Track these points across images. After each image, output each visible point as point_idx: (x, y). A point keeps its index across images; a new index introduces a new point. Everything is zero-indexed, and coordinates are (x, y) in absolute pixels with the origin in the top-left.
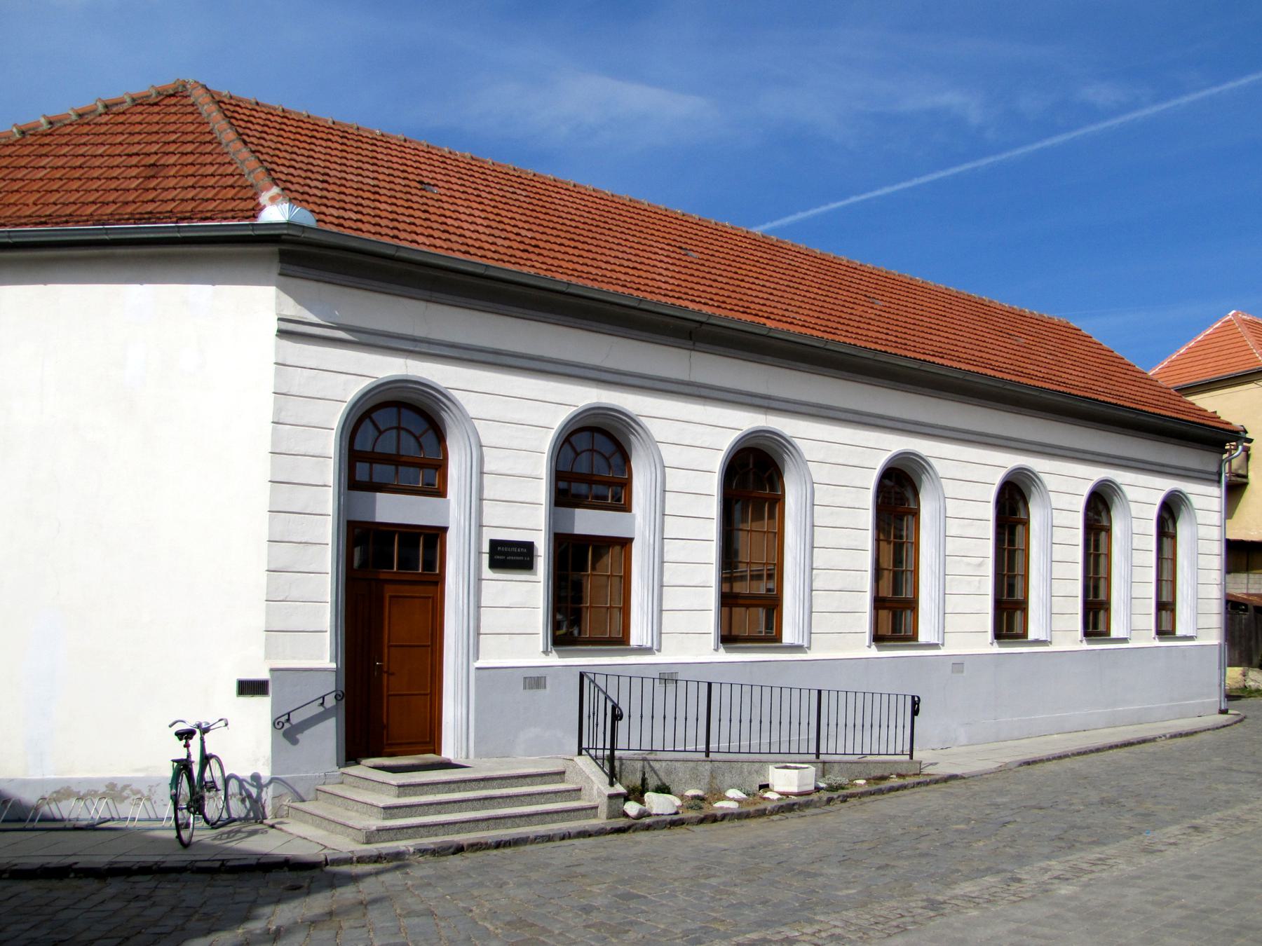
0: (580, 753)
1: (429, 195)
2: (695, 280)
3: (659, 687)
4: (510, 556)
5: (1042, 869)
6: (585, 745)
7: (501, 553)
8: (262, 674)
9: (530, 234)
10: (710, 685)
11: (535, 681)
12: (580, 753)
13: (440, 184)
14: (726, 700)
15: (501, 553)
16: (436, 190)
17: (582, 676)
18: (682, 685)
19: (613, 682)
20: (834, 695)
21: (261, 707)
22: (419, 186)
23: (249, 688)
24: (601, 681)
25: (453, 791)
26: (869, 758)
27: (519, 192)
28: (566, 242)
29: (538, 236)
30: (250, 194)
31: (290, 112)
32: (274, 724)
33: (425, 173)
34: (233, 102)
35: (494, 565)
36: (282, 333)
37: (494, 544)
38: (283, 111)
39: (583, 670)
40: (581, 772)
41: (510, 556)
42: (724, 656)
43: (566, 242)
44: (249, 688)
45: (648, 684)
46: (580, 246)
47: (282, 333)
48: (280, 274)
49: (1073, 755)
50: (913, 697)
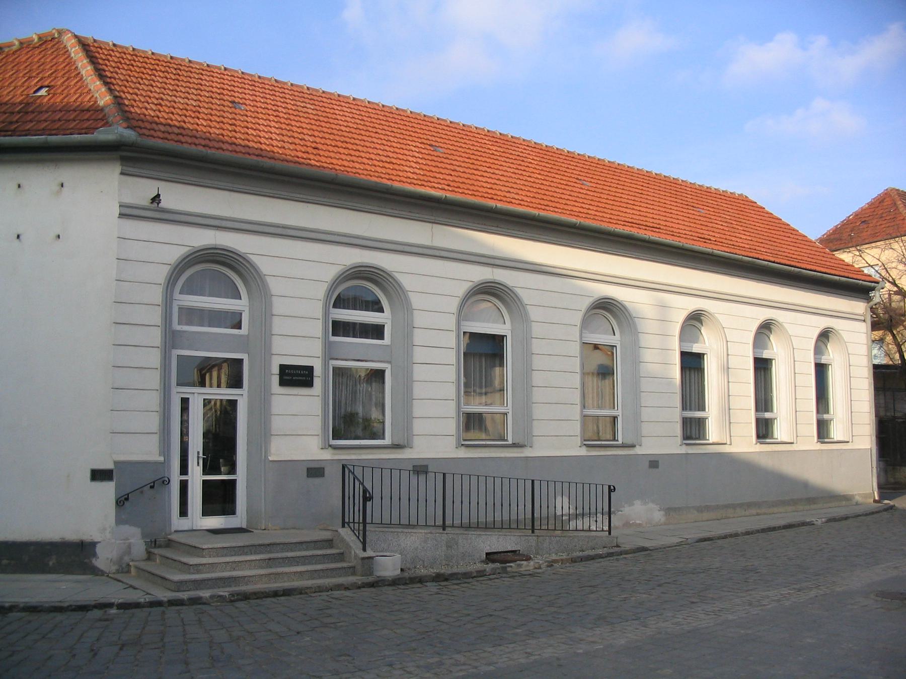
0: (343, 526)
1: (237, 111)
2: (484, 159)
3: (414, 479)
4: (296, 376)
5: (354, 574)
6: (347, 520)
7: (288, 375)
8: (109, 466)
9: (369, 120)
10: (533, 481)
11: (315, 471)
12: (343, 526)
13: (248, 102)
14: (544, 491)
15: (288, 375)
16: (243, 107)
17: (344, 467)
18: (431, 476)
19: (368, 472)
20: (544, 484)
21: (108, 490)
22: (230, 105)
23: (99, 475)
24: (358, 472)
25: (246, 554)
26: (593, 534)
27: (308, 106)
28: (339, 144)
29: (318, 140)
30: (100, 116)
31: (139, 51)
32: (117, 502)
33: (236, 94)
34: (96, 45)
35: (283, 383)
36: (122, 215)
37: (283, 368)
38: (134, 49)
39: (344, 463)
40: (343, 540)
41: (296, 376)
42: (463, 453)
43: (339, 144)
44: (99, 475)
45: (405, 475)
46: (350, 146)
47: (122, 215)
48: (122, 173)
49: (758, 531)
50: (609, 486)
